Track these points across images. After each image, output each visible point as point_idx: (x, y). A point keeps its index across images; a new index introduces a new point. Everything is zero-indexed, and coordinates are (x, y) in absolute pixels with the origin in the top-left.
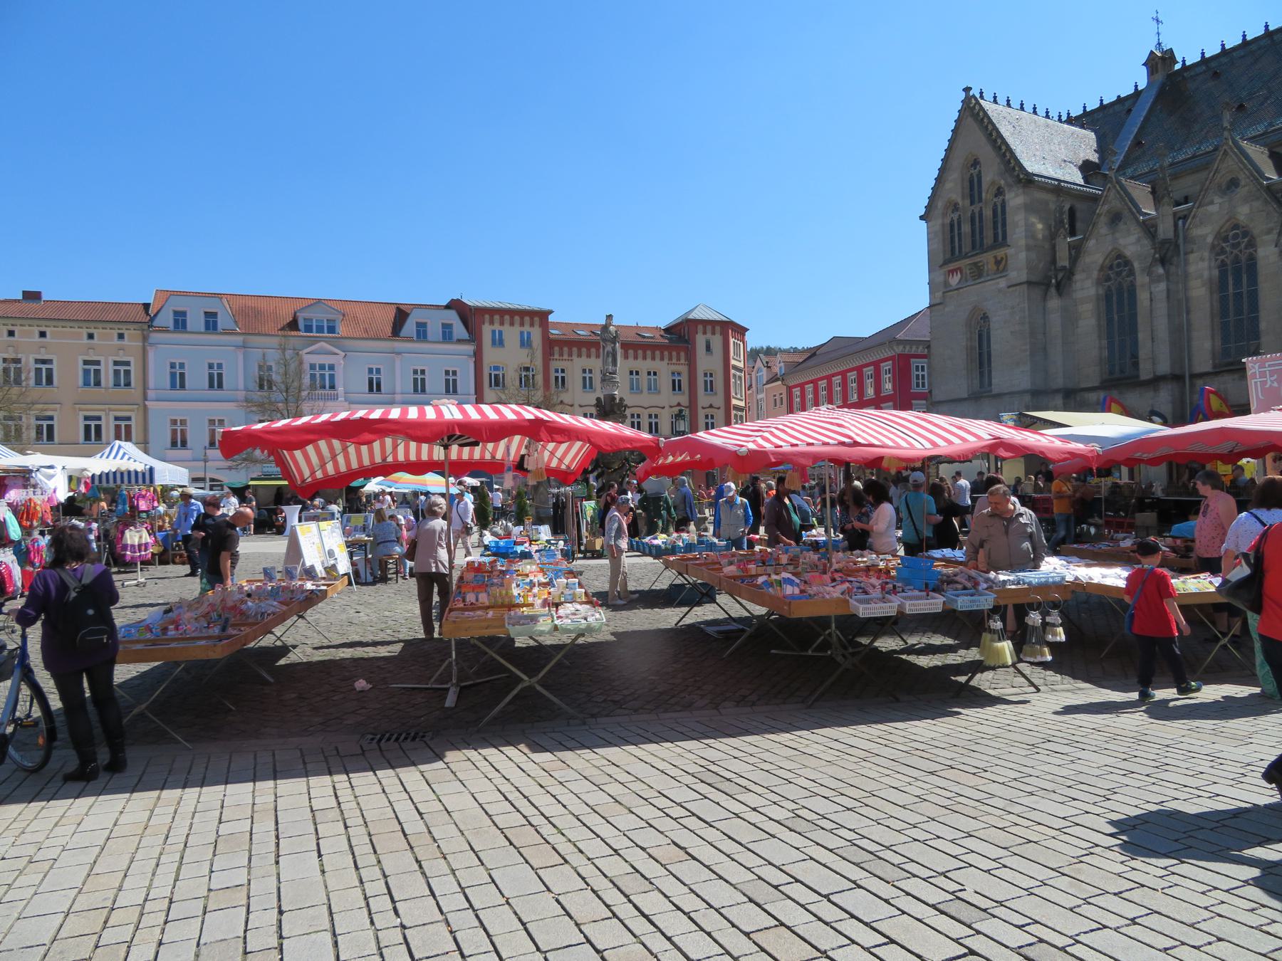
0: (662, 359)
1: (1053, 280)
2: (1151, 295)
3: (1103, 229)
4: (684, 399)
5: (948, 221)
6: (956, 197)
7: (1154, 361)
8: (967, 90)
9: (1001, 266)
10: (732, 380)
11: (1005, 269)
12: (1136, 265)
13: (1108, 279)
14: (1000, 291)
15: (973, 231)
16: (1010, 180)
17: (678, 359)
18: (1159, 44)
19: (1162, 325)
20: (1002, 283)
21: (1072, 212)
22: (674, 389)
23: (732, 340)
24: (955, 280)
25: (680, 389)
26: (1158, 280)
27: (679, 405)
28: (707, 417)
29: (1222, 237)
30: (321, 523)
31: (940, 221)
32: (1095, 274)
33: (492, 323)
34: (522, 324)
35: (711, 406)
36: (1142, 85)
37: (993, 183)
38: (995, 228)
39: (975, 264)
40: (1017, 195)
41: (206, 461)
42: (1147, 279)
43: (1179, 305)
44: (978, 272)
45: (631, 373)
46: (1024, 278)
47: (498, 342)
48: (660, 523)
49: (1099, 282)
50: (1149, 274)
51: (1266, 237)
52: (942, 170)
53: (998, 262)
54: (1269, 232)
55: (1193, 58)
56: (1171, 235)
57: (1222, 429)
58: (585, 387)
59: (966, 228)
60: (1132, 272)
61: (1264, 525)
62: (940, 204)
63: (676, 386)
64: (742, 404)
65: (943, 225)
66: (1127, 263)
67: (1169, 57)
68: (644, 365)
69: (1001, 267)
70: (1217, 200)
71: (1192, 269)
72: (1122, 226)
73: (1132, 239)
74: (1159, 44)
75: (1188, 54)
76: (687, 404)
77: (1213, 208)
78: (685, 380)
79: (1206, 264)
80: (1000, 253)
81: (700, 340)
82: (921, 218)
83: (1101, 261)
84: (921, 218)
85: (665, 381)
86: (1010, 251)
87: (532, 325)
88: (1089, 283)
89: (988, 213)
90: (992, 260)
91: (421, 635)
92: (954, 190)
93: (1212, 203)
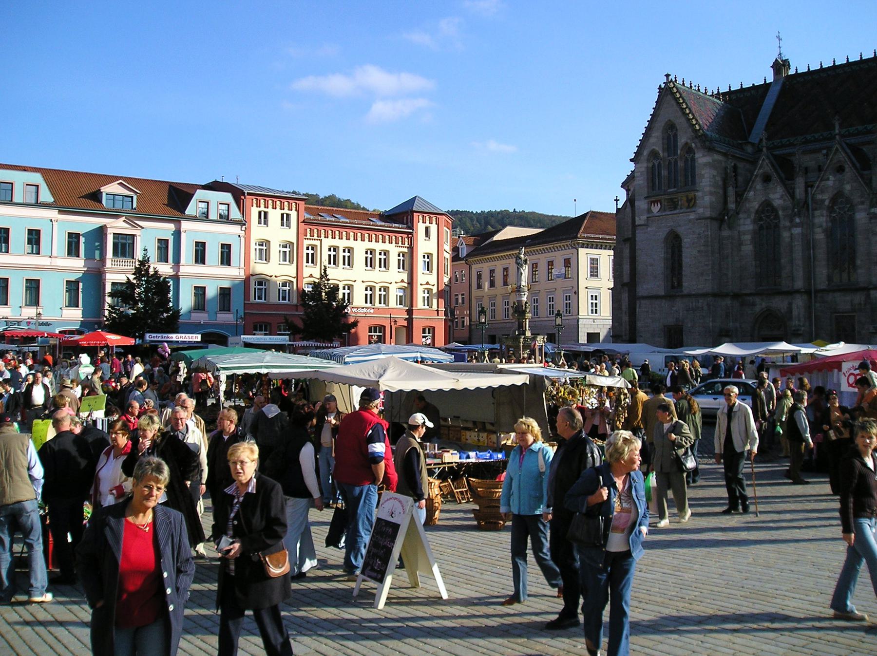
0: (390, 242)
1: (723, 217)
2: (791, 233)
3: (759, 186)
5: (650, 165)
6: (659, 149)
7: (792, 278)
8: (667, 76)
9: (691, 203)
11: (694, 205)
12: (780, 213)
13: (761, 219)
14: (690, 221)
16: (699, 145)
17: (403, 243)
18: (780, 54)
19: (798, 254)
20: (692, 216)
21: (735, 168)
24: (656, 209)
26: (797, 225)
27: (428, 283)
29: (834, 200)
31: (645, 165)
32: (753, 216)
33: (424, 222)
34: (282, 208)
35: (428, 283)
36: (770, 79)
37: (686, 144)
38: (686, 177)
39: (672, 199)
40: (704, 156)
41: (808, 292)
42: (788, 224)
43: (809, 244)
44: (673, 205)
46: (708, 213)
47: (264, 218)
49: (754, 222)
50: (791, 221)
51: (860, 207)
52: (649, 129)
53: (689, 201)
54: (862, 203)
55: (803, 69)
56: (803, 196)
57: (208, 456)
59: (664, 173)
60: (777, 217)
61: (529, 596)
62: (645, 153)
65: (647, 167)
66: (774, 210)
67: (786, 64)
69: (691, 205)
70: (831, 177)
71: (816, 221)
72: (771, 185)
73: (778, 196)
74: (780, 54)
75: (799, 64)
77: (830, 183)
79: (824, 219)
80: (691, 195)
81: (420, 227)
82: (631, 160)
83: (757, 207)
84: (631, 160)
86: (699, 194)
88: (748, 221)
89: (681, 164)
90: (685, 199)
92: (656, 143)
93: (828, 179)
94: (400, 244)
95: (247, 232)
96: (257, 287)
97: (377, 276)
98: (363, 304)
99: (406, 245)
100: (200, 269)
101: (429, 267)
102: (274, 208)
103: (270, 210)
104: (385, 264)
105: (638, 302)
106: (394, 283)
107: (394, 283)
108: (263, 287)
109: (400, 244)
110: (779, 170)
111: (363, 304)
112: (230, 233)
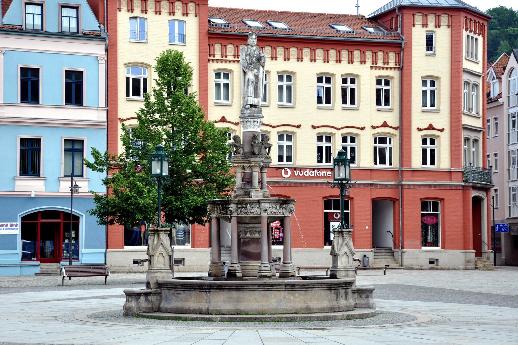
4: (393, 119)
10: (465, 91)
15: (248, 88)
22: (379, 103)
23: (465, 33)
25: (387, 102)
27: (431, 127)
28: (424, 142)
30: (355, 13)
33: (425, 25)
34: (172, 13)
35: (431, 127)
45: (320, 80)
48: (160, 82)
58: (344, 102)
63: (382, 98)
64: (478, 123)
68: (338, 69)
76: (396, 124)
78: (394, 89)
81: (418, 35)
85: (366, 90)
87: (185, 14)
91: (109, 226)
94: (380, 64)
95: (111, 52)
96: (378, 145)
97: (338, 116)
98: (313, 162)
99: (392, 64)
100: (74, 114)
101: (430, 99)
102: (158, 12)
103: (151, 15)
104: (349, 96)
105: (73, 213)
106: (368, 129)
107: (368, 129)
108: (388, 145)
109: (380, 64)
110: (437, 342)
111: (313, 162)
112: (86, 56)
